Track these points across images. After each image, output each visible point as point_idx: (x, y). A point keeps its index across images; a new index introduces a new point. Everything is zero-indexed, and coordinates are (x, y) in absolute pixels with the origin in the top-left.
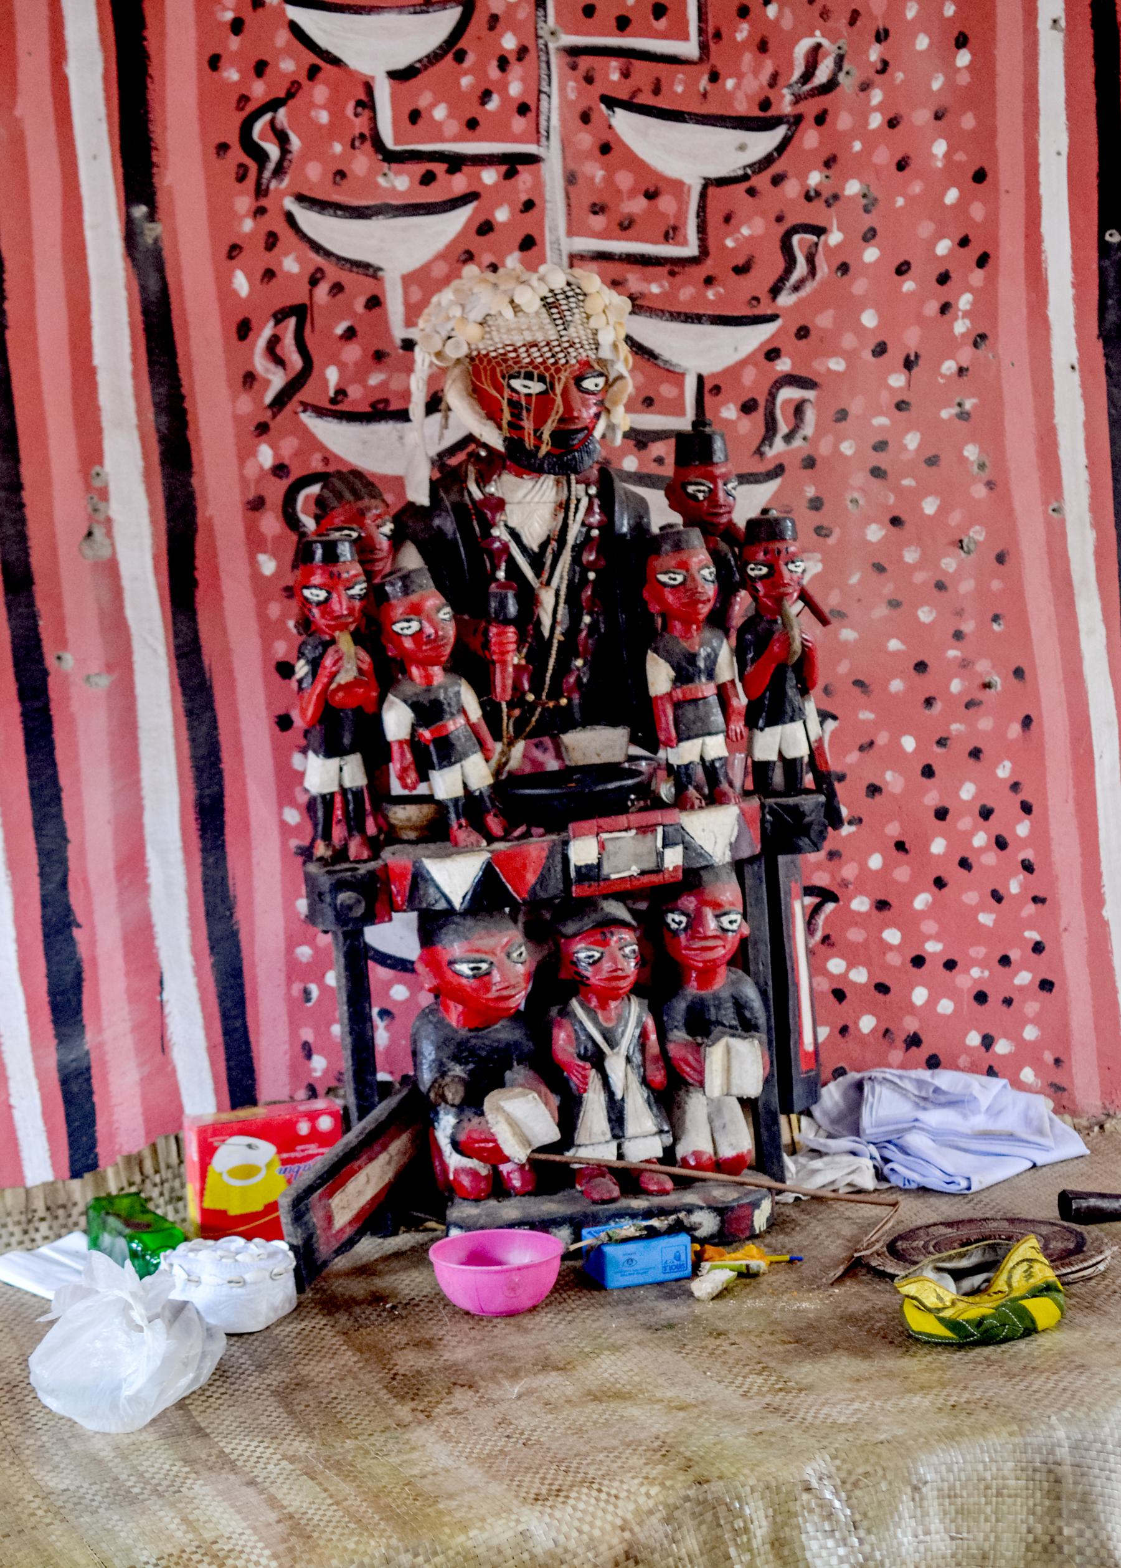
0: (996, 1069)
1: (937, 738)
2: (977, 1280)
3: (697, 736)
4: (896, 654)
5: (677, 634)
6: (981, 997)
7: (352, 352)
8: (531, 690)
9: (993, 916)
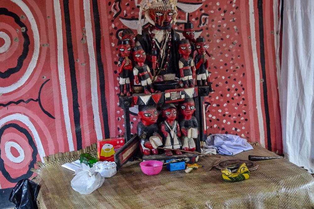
0: (237, 134)
1: (228, 77)
2: (235, 170)
3: (187, 76)
4: (222, 62)
5: (184, 58)
6: (235, 122)
7: (128, 8)
8: (159, 67)
9: (237, 108)
